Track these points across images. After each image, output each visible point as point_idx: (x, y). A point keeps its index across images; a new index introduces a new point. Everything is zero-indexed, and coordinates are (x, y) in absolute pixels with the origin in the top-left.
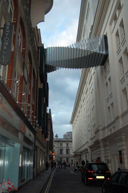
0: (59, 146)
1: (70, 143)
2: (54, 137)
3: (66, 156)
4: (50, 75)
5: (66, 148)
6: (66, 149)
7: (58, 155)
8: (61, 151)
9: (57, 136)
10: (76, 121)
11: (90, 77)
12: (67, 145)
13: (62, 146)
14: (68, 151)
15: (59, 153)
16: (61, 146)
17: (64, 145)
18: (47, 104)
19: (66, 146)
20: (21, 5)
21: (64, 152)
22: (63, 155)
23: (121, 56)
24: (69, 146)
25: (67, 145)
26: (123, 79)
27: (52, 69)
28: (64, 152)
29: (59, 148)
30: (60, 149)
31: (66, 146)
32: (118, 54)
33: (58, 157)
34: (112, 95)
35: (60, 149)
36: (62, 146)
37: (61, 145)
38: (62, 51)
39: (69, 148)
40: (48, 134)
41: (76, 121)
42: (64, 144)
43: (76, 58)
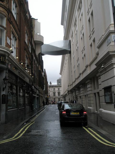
0: (53, 90)
1: (60, 88)
2: (49, 84)
3: (57, 97)
4: (43, 57)
5: (58, 91)
6: (58, 92)
7: (52, 97)
8: (54, 93)
9: (51, 83)
10: (65, 64)
11: (72, 33)
12: (59, 89)
13: (55, 90)
14: (59, 93)
15: (53, 95)
16: (54, 90)
17: (56, 89)
18: (42, 59)
19: (58, 90)
20: (32, 122)
21: (57, 94)
22: (55, 97)
23: (90, 17)
24: (60, 90)
25: (59, 89)
26: (93, 31)
27: (43, 55)
28: (57, 94)
29: (53, 92)
30: (53, 93)
31: (58, 90)
32: (88, 14)
33: (52, 98)
34: (94, 29)
35: (53, 93)
36: (55, 90)
37: (54, 89)
38: (48, 46)
39: (60, 92)
40: (44, 87)
41: (65, 64)
42: (56, 88)
43: (55, 51)
